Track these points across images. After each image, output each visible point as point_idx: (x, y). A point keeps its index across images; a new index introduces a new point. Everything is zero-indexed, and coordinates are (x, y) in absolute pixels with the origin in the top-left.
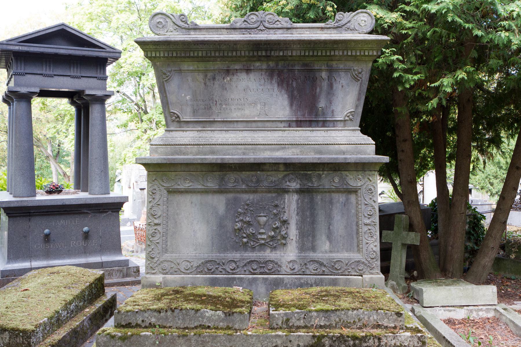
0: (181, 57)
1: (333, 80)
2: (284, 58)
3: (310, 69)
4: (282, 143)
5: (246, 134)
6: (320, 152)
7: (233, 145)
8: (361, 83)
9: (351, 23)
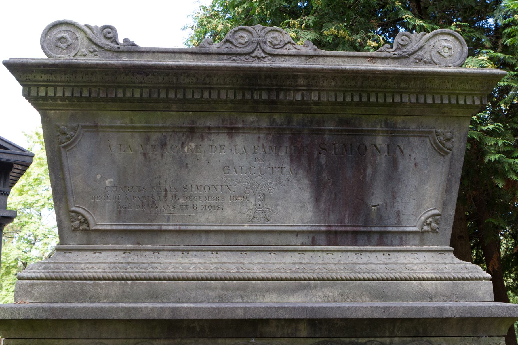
0: (97, 100)
1: (398, 152)
2: (302, 107)
3: (353, 131)
4: (302, 275)
5: (224, 258)
6: (382, 296)
7: (198, 279)
8: (451, 160)
9: (425, 50)
